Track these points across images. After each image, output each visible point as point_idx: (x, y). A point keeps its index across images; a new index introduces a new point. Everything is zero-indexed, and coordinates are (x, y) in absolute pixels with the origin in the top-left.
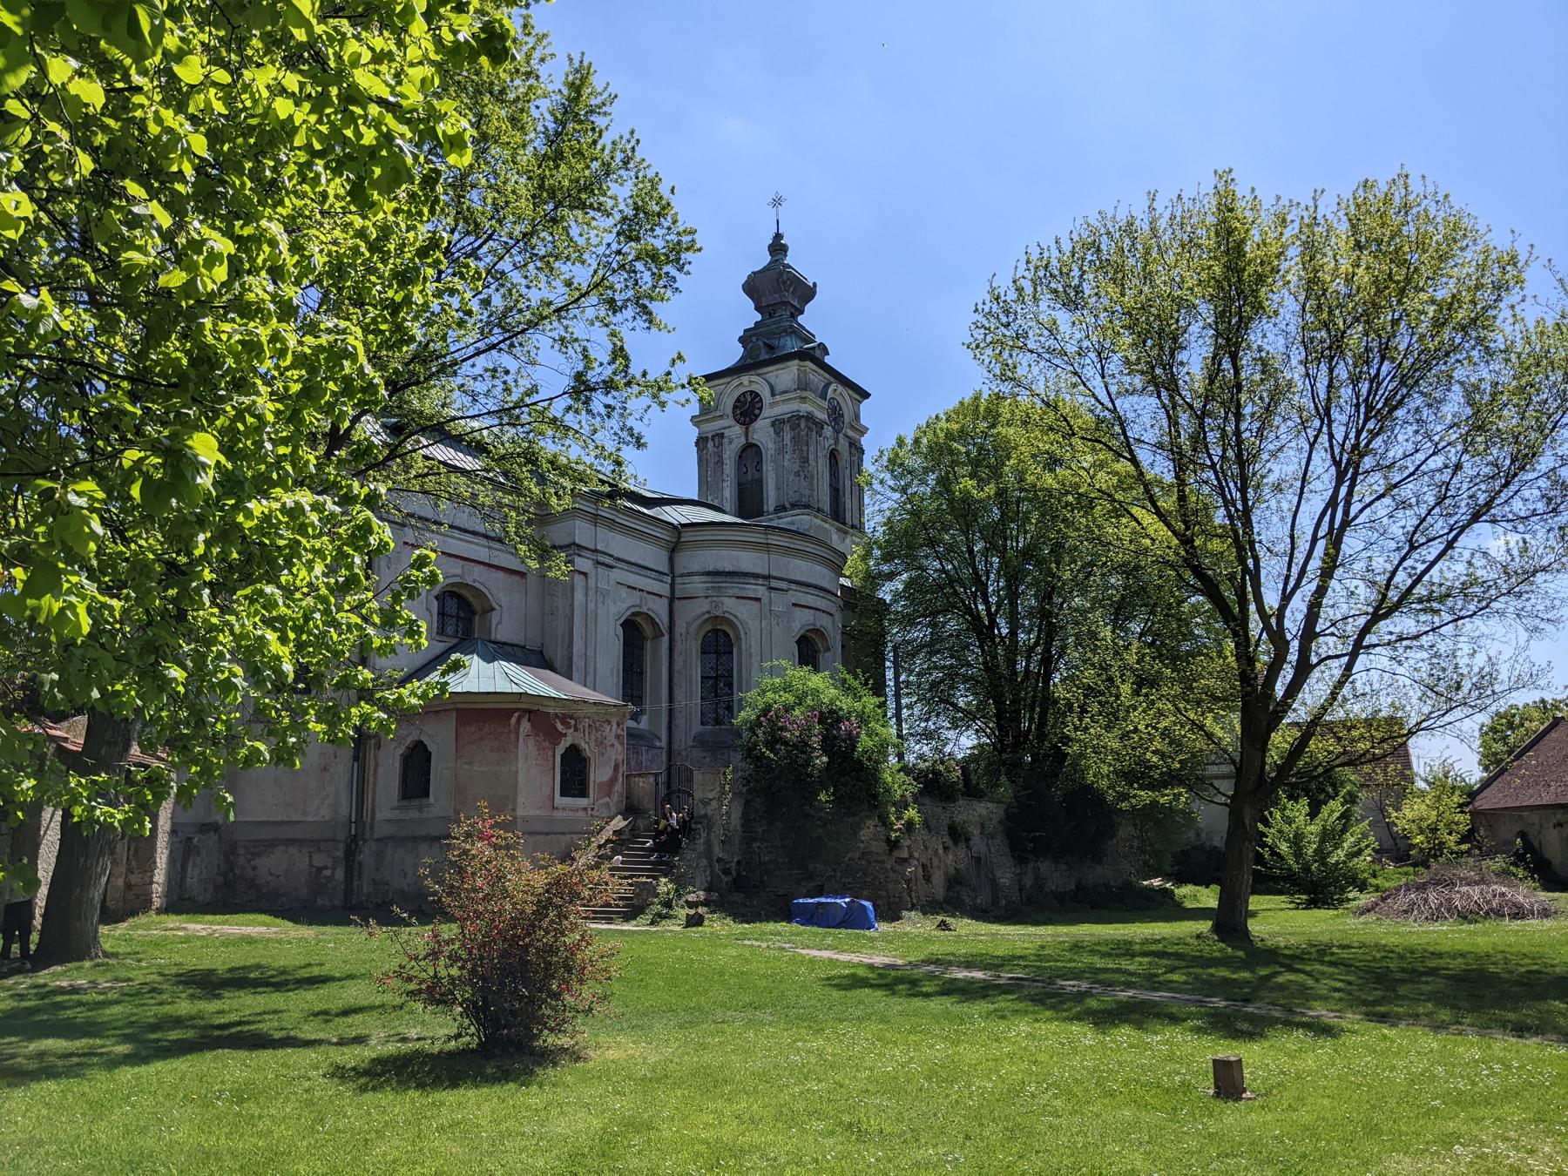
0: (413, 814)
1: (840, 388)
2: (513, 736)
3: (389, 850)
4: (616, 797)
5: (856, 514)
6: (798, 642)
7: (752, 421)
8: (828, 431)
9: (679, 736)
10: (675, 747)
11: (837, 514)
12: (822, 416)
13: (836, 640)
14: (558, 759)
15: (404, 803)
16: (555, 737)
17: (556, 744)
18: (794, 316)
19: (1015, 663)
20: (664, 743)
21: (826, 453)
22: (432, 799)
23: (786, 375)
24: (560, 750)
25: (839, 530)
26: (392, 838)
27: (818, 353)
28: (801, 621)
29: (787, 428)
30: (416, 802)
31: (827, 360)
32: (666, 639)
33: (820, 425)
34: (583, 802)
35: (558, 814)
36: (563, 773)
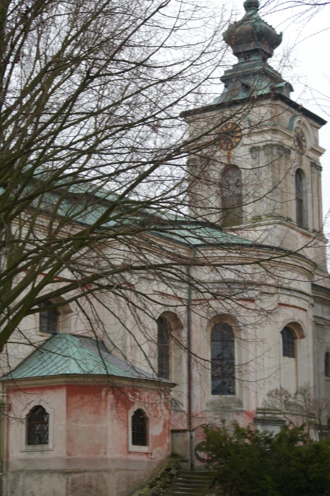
0: (37, 455)
1: (304, 119)
2: (103, 404)
3: (21, 479)
4: (166, 447)
5: (316, 220)
6: (282, 332)
7: (233, 147)
8: (293, 155)
9: (196, 402)
10: (194, 411)
11: (301, 222)
12: (289, 143)
13: (308, 328)
14: (130, 419)
15: (30, 447)
16: (127, 405)
17: (128, 409)
18: (264, 60)
19: (36, 85)
20: (185, 408)
21: (293, 172)
22: (50, 445)
23: (261, 112)
24: (131, 413)
25: (304, 234)
26: (22, 471)
27: (284, 93)
28: (285, 317)
29: (262, 153)
30: (39, 447)
31: (293, 97)
32: (186, 329)
33: (288, 151)
34: (144, 449)
35: (132, 457)
36: (133, 429)
